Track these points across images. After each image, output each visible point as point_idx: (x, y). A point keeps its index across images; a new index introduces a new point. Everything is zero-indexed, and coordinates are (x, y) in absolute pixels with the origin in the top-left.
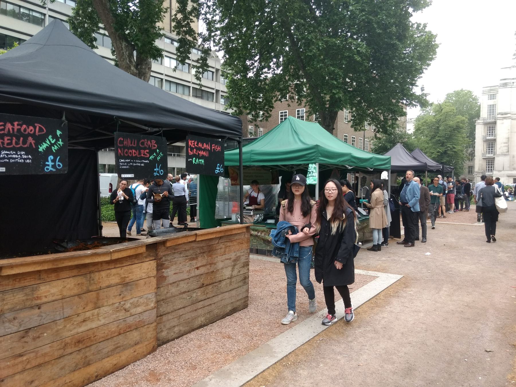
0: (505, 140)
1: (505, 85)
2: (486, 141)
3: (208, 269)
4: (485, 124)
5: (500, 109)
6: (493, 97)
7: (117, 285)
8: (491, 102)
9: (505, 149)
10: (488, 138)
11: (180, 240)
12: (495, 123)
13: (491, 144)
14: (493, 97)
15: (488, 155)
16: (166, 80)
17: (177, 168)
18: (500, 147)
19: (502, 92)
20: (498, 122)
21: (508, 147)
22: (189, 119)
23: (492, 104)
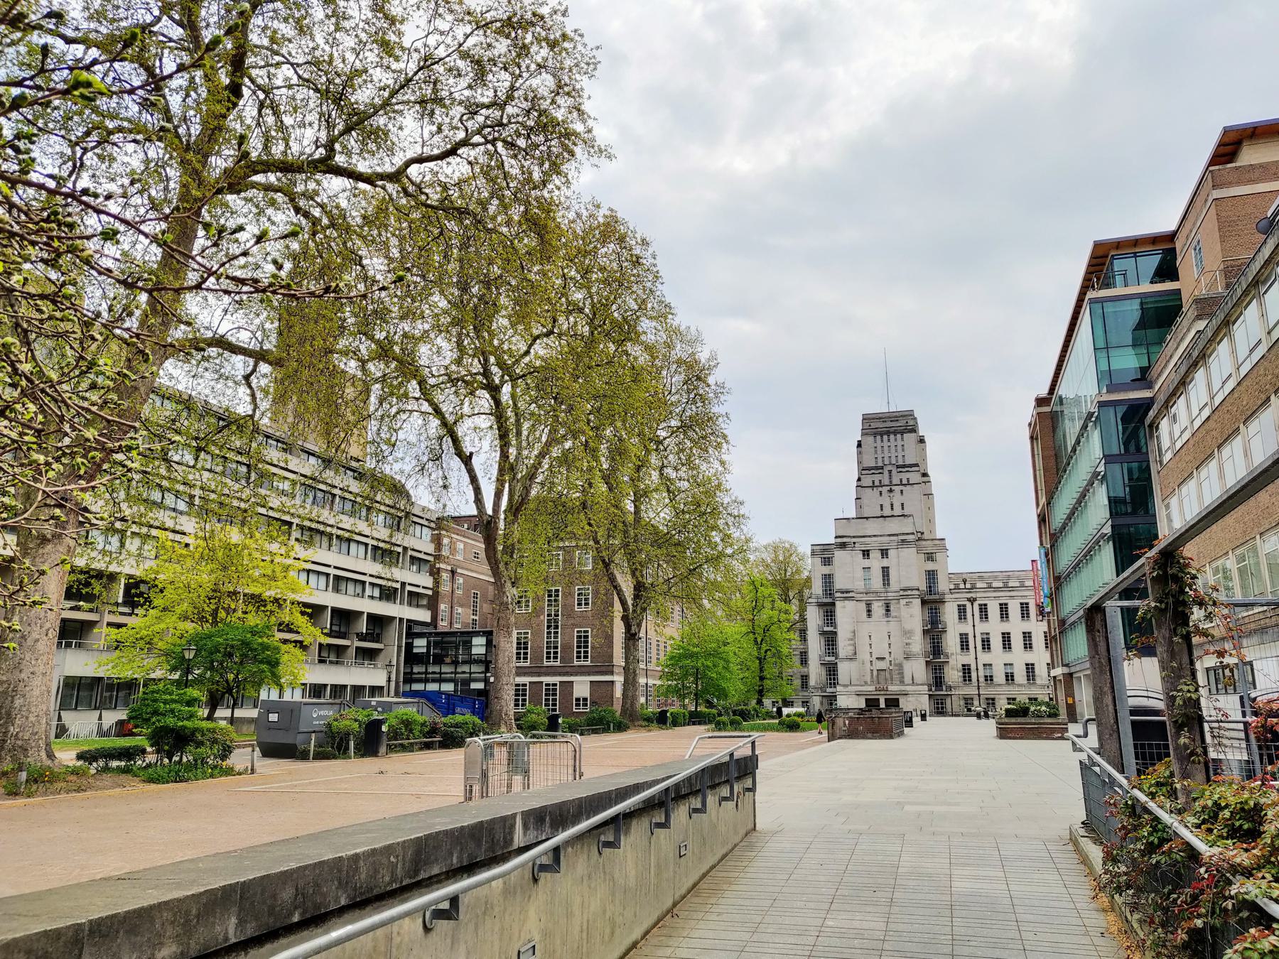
0: (850, 635)
1: (843, 546)
2: (823, 633)
3: (478, 782)
4: (820, 605)
5: (839, 584)
6: (827, 561)
7: (170, 76)
8: (826, 570)
9: (850, 650)
10: (826, 629)
11: (1263, 249)
12: (833, 604)
13: (830, 639)
14: (827, 561)
15: (828, 659)
16: (371, 584)
17: (408, 621)
18: (843, 648)
19: (839, 555)
20: (838, 603)
21: (854, 645)
22: (283, 941)
23: (827, 572)
